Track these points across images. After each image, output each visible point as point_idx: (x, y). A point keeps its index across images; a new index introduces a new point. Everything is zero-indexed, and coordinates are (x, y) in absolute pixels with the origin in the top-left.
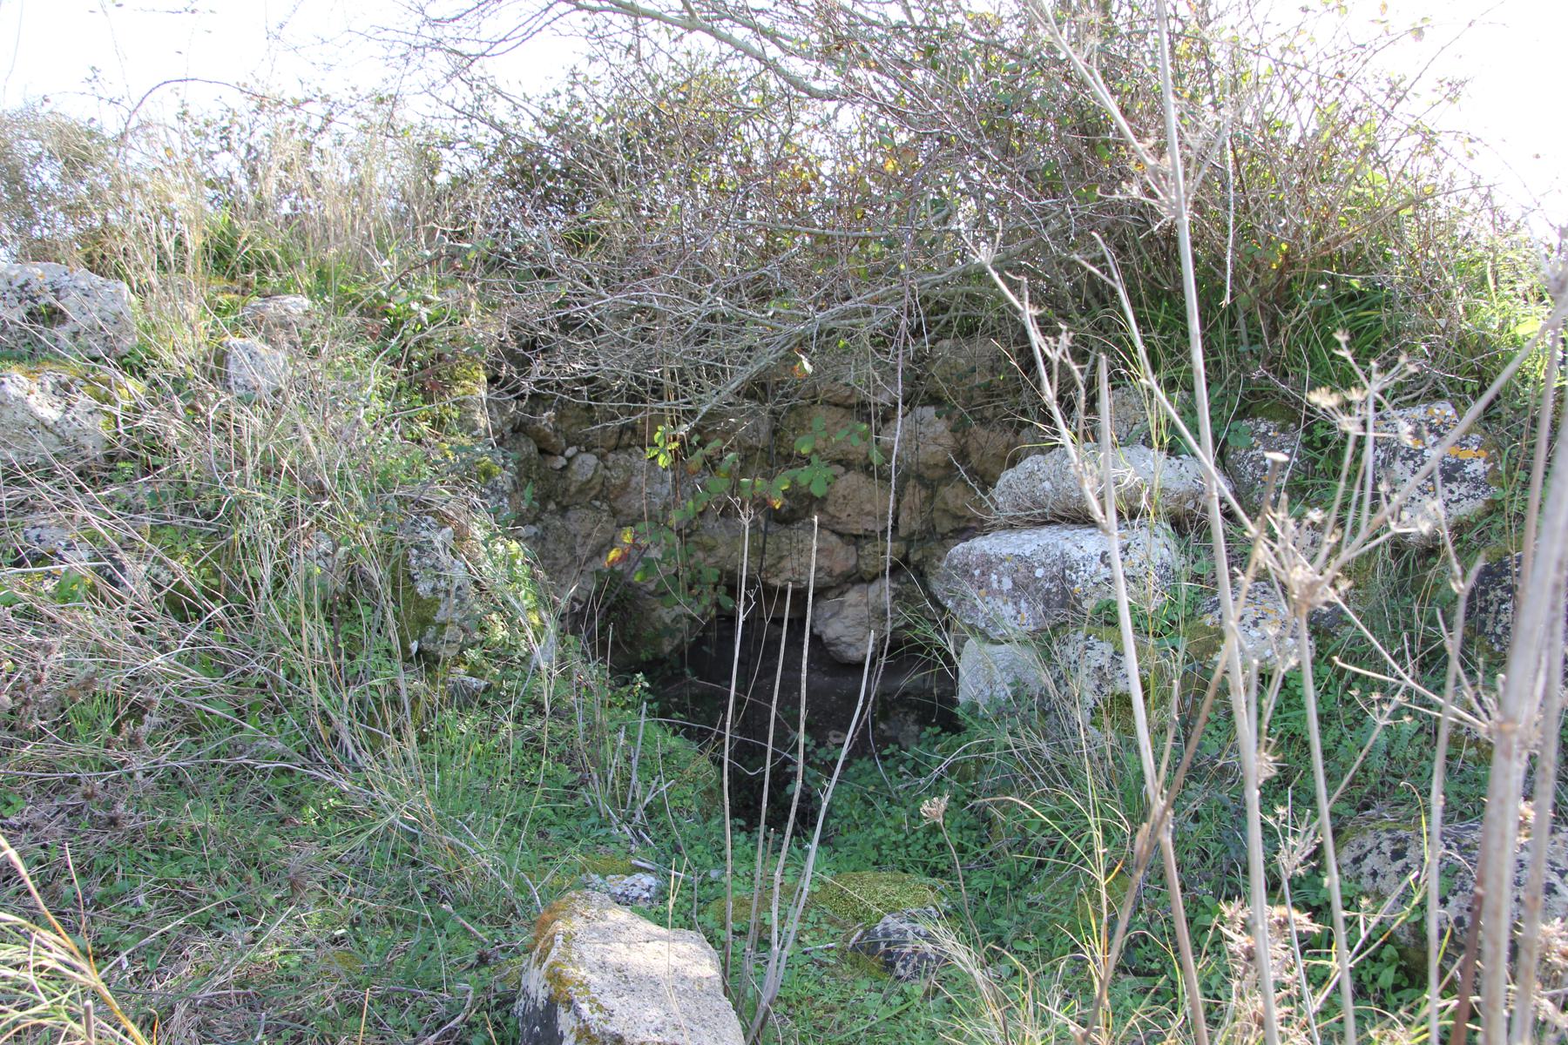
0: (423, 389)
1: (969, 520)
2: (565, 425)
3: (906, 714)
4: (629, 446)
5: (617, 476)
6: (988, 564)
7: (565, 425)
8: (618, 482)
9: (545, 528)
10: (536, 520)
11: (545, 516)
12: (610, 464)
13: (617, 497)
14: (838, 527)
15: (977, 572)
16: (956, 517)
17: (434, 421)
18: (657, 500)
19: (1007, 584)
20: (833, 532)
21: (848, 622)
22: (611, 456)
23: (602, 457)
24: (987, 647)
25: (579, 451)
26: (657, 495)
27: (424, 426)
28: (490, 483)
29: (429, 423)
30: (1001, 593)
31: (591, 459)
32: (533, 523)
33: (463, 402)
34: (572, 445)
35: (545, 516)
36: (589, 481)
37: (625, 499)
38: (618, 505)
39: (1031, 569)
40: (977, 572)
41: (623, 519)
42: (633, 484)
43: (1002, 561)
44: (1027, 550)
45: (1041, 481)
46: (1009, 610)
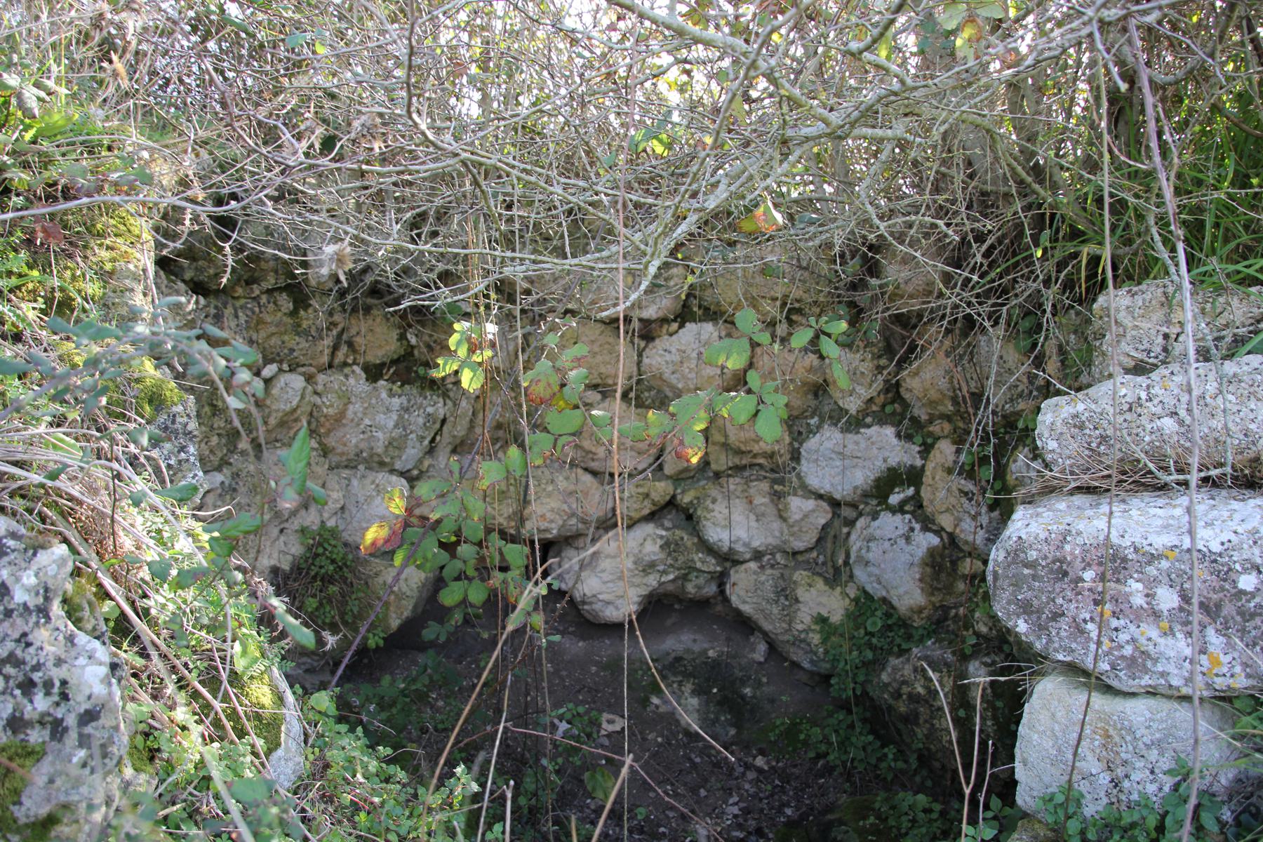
0: (29, 242)
1: (755, 456)
2: (263, 334)
3: (680, 684)
4: (345, 364)
5: (330, 406)
6: (1114, 563)
7: (263, 334)
8: (331, 411)
9: (236, 475)
10: (223, 463)
11: (234, 459)
12: (320, 388)
13: (329, 431)
14: (594, 465)
15: (1089, 575)
16: (739, 452)
17: (49, 301)
18: (380, 435)
19: (1168, 599)
20: (586, 469)
21: (606, 577)
22: (321, 378)
23: (309, 379)
24: (1100, 702)
25: (281, 370)
26: (380, 428)
27: (29, 311)
28: (162, 418)
29: (41, 304)
30: (1156, 615)
31: (297, 381)
32: (219, 469)
33: (111, 274)
34: (272, 361)
35: (234, 459)
36: (295, 410)
37: (339, 434)
38: (331, 441)
39: (1226, 575)
40: (1089, 575)
41: (335, 459)
42: (350, 414)
43: (1153, 558)
44: (1211, 539)
45: (1155, 417)
46: (1180, 646)
